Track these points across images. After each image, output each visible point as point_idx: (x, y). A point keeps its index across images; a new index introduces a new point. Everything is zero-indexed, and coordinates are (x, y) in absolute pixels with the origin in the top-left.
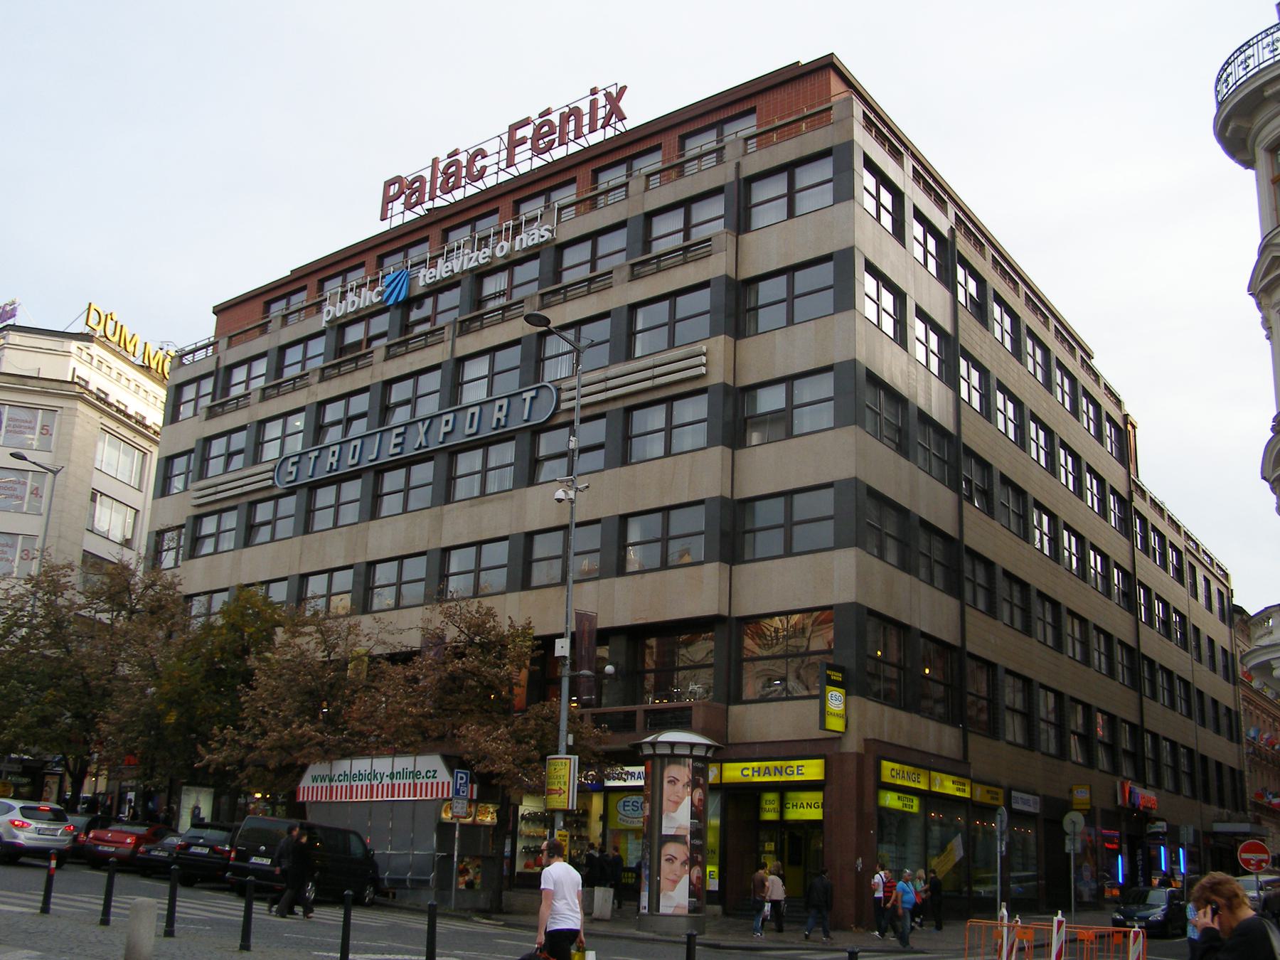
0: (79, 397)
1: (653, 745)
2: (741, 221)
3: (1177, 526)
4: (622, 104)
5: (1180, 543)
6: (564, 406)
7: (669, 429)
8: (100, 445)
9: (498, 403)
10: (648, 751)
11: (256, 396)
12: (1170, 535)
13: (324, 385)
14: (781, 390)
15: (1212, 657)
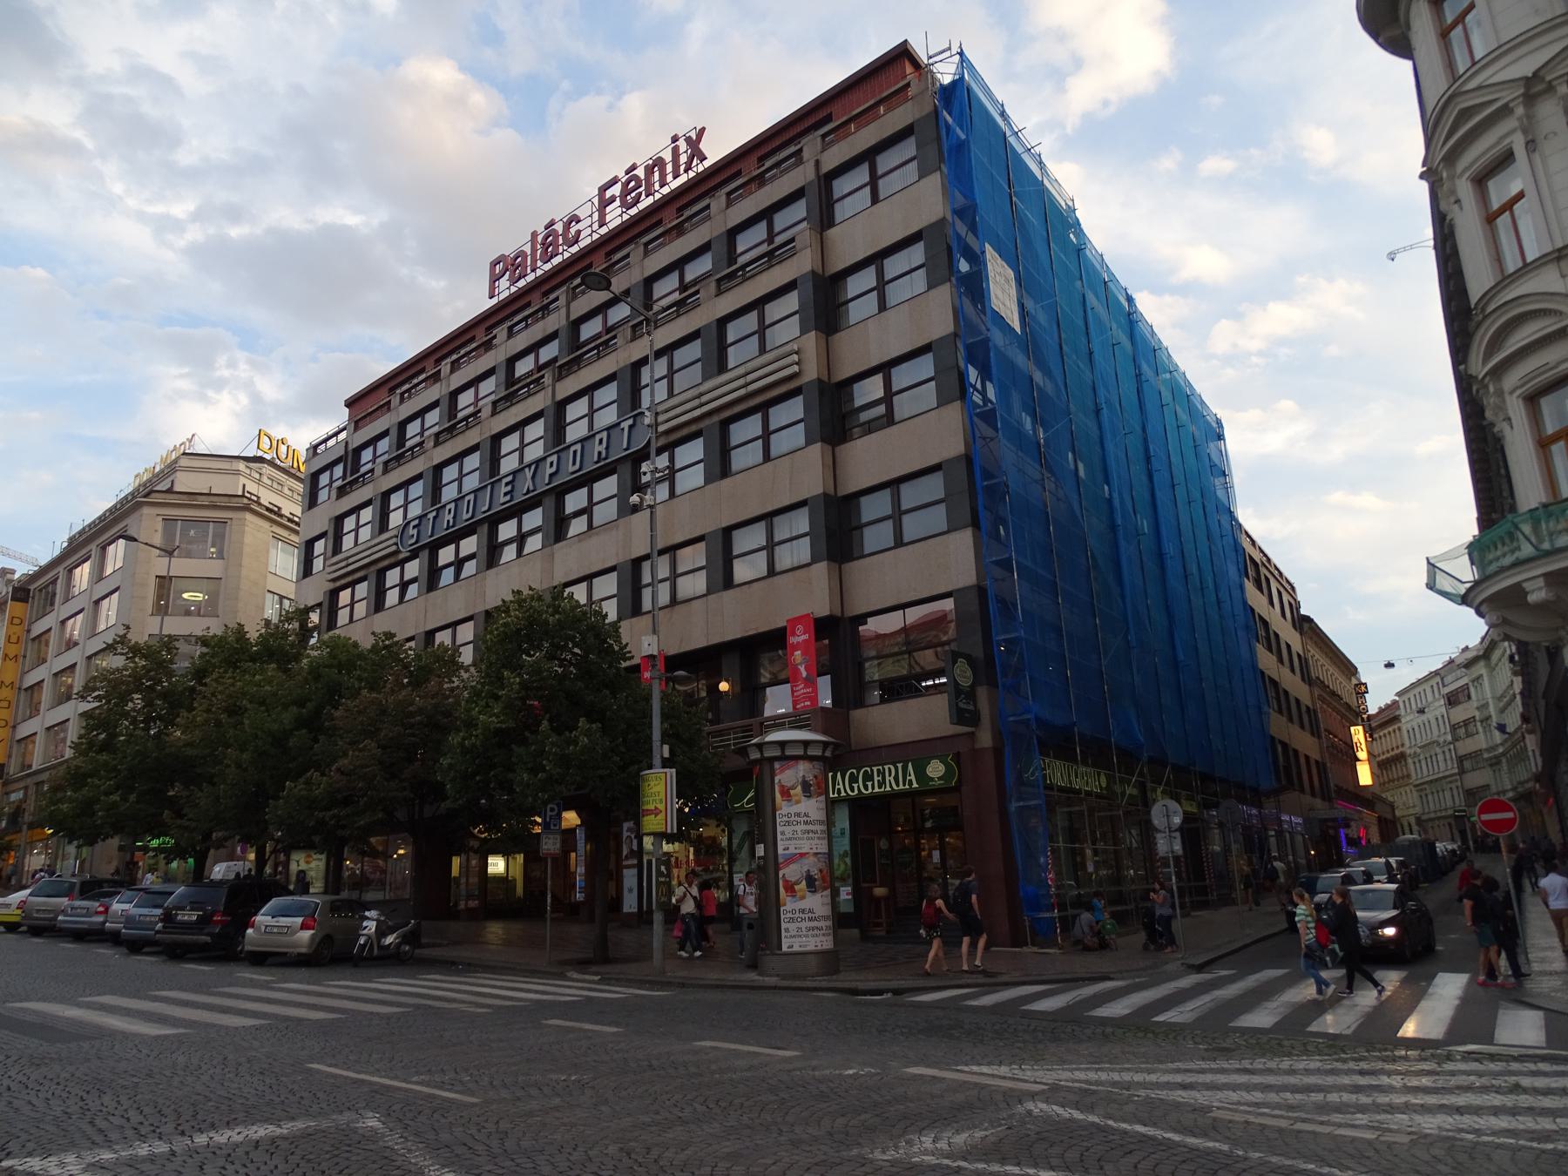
0: (247, 508)
1: (760, 746)
2: (824, 218)
3: (1253, 542)
5: (1257, 557)
7: (766, 435)
8: (273, 552)
9: (598, 437)
10: (755, 755)
11: (379, 470)
13: (439, 449)
14: (878, 379)
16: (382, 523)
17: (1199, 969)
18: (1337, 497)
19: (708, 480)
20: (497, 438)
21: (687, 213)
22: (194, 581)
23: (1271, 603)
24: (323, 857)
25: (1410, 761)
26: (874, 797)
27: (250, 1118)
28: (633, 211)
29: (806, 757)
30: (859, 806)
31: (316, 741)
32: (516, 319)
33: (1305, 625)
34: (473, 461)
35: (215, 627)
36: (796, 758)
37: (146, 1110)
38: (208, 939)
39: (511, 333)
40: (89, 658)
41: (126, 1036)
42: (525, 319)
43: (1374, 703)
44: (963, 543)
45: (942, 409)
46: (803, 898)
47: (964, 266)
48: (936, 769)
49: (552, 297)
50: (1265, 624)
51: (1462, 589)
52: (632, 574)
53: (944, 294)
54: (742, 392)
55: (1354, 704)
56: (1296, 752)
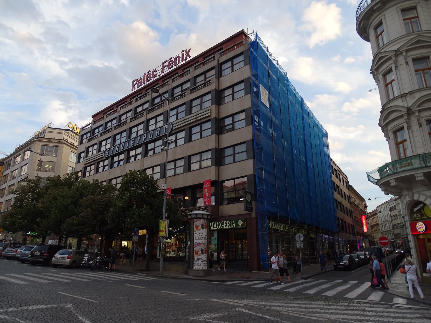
0: (64, 143)
1: (191, 215)
2: (219, 75)
3: (336, 165)
4: (190, 53)
5: (336, 168)
6: (174, 128)
7: (201, 131)
8: (71, 155)
9: (157, 130)
10: (189, 217)
11: (99, 135)
12: (334, 166)
13: (116, 130)
15: (345, 197)
16: (99, 149)
17: (305, 279)
18: (372, 152)
19: (185, 143)
20: (131, 128)
21: (185, 71)
22: (48, 162)
23: (340, 181)
24: (77, 239)
25: (380, 225)
26: (224, 229)
27: (39, 304)
28: (171, 70)
29: (203, 218)
30: (221, 232)
31: (76, 208)
32: (138, 96)
33: (350, 187)
34: (124, 134)
35: (52, 175)
36: (200, 218)
37: (14, 301)
38: (42, 260)
39: (137, 100)
40: (19, 182)
41: (14, 283)
42: (140, 97)
43: (370, 209)
44: (250, 163)
45: (247, 127)
46: (200, 255)
47: (255, 89)
48: (240, 223)
49: (148, 91)
50: (338, 187)
51: (376, 181)
52: (164, 167)
53: (249, 96)
54: (195, 120)
55: (363, 209)
56: (345, 222)
